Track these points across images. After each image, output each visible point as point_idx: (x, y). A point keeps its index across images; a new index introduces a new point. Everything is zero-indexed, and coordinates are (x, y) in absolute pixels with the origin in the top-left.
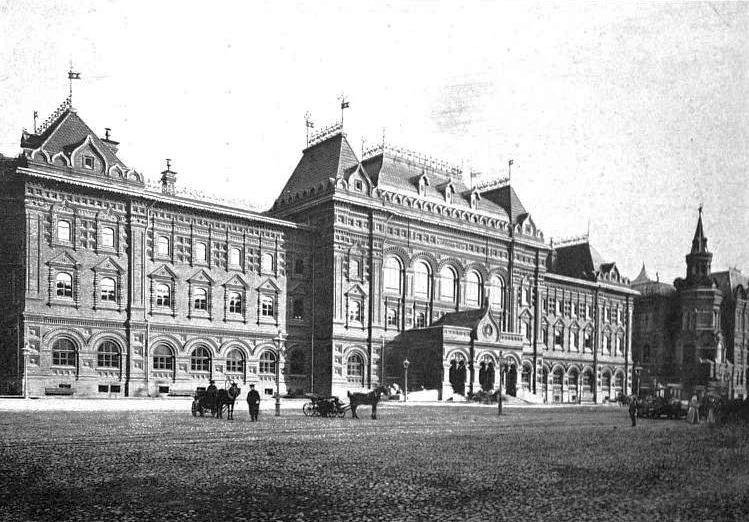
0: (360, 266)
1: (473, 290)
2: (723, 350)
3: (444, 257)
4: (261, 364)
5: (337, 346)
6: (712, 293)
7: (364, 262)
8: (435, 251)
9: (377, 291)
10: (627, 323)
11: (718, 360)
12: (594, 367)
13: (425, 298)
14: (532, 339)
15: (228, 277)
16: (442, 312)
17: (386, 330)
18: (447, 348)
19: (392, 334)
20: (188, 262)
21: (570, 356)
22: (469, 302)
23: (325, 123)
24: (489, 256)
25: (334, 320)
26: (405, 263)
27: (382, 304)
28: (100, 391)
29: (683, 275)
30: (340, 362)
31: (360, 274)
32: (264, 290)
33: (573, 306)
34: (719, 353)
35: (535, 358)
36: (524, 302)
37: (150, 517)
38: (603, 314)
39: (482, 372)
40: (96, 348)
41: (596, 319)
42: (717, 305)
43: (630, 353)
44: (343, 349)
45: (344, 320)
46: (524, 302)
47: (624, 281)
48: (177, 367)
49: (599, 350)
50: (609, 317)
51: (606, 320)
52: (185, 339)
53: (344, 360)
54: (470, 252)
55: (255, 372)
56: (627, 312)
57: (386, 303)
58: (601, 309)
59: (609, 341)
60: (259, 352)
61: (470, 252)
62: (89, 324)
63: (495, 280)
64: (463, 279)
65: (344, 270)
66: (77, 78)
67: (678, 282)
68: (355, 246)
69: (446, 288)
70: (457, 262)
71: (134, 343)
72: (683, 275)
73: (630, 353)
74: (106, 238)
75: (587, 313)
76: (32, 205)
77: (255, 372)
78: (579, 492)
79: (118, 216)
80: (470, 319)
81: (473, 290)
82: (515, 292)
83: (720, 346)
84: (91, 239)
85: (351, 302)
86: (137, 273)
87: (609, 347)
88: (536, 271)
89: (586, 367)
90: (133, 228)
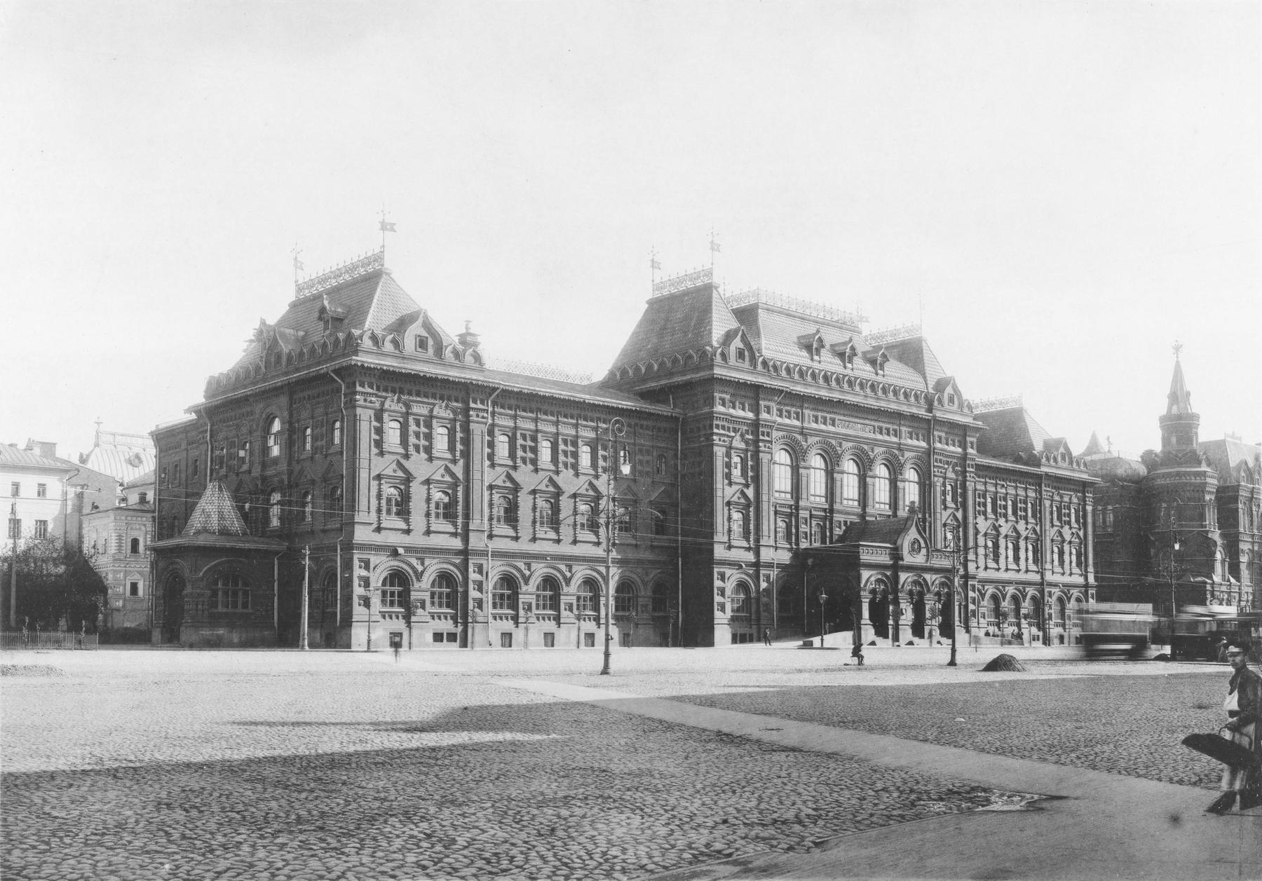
0: (744, 461)
1: (783, 475)
2: (1223, 561)
3: (846, 445)
4: (433, 595)
5: (361, 560)
6: (1204, 474)
7: (458, 428)
8: (835, 438)
9: (765, 498)
10: (1085, 524)
11: (1217, 578)
12: (1042, 592)
13: (787, 498)
14: (460, 521)
15: (580, 485)
16: (845, 522)
17: (776, 548)
18: (865, 574)
19: (785, 557)
20: (426, 456)
21: (1011, 576)
22: (812, 498)
23: (679, 267)
24: (806, 425)
25: (716, 539)
26: (797, 456)
27: (772, 513)
28: (435, 640)
29: (1157, 447)
30: (480, 589)
31: (452, 448)
32: (498, 487)
33: (989, 500)
34: (1218, 566)
35: (466, 562)
36: (950, 504)
37: (5, 820)
38: (1052, 513)
39: (872, 603)
40: (380, 584)
41: (1040, 521)
42: (1210, 493)
43: (1091, 569)
44: (372, 566)
45: (725, 539)
46: (950, 504)
47: (1078, 464)
48: (562, 606)
49: (1048, 566)
50: (1059, 519)
51: (1056, 523)
52: (423, 564)
53: (728, 592)
54: (879, 437)
55: (571, 610)
56: (1084, 510)
57: (776, 513)
58: (1048, 510)
59: (1061, 553)
60: (577, 581)
61: (879, 437)
62: (530, 557)
63: (911, 474)
64: (802, 464)
65: (374, 436)
66: (393, 230)
67: (1148, 459)
68: (738, 437)
69: (849, 488)
70: (862, 450)
71: (473, 576)
72: (1157, 447)
73: (1091, 569)
74: (441, 443)
75: (1073, 519)
76: (361, 402)
77: (571, 610)
78: (376, 799)
79: (454, 411)
80: (891, 531)
81: (783, 475)
82: (938, 489)
83: (1218, 556)
84: (423, 442)
85: (496, 497)
86: (476, 486)
87: (1062, 562)
88: (964, 457)
89: (1031, 591)
90: (472, 426)
